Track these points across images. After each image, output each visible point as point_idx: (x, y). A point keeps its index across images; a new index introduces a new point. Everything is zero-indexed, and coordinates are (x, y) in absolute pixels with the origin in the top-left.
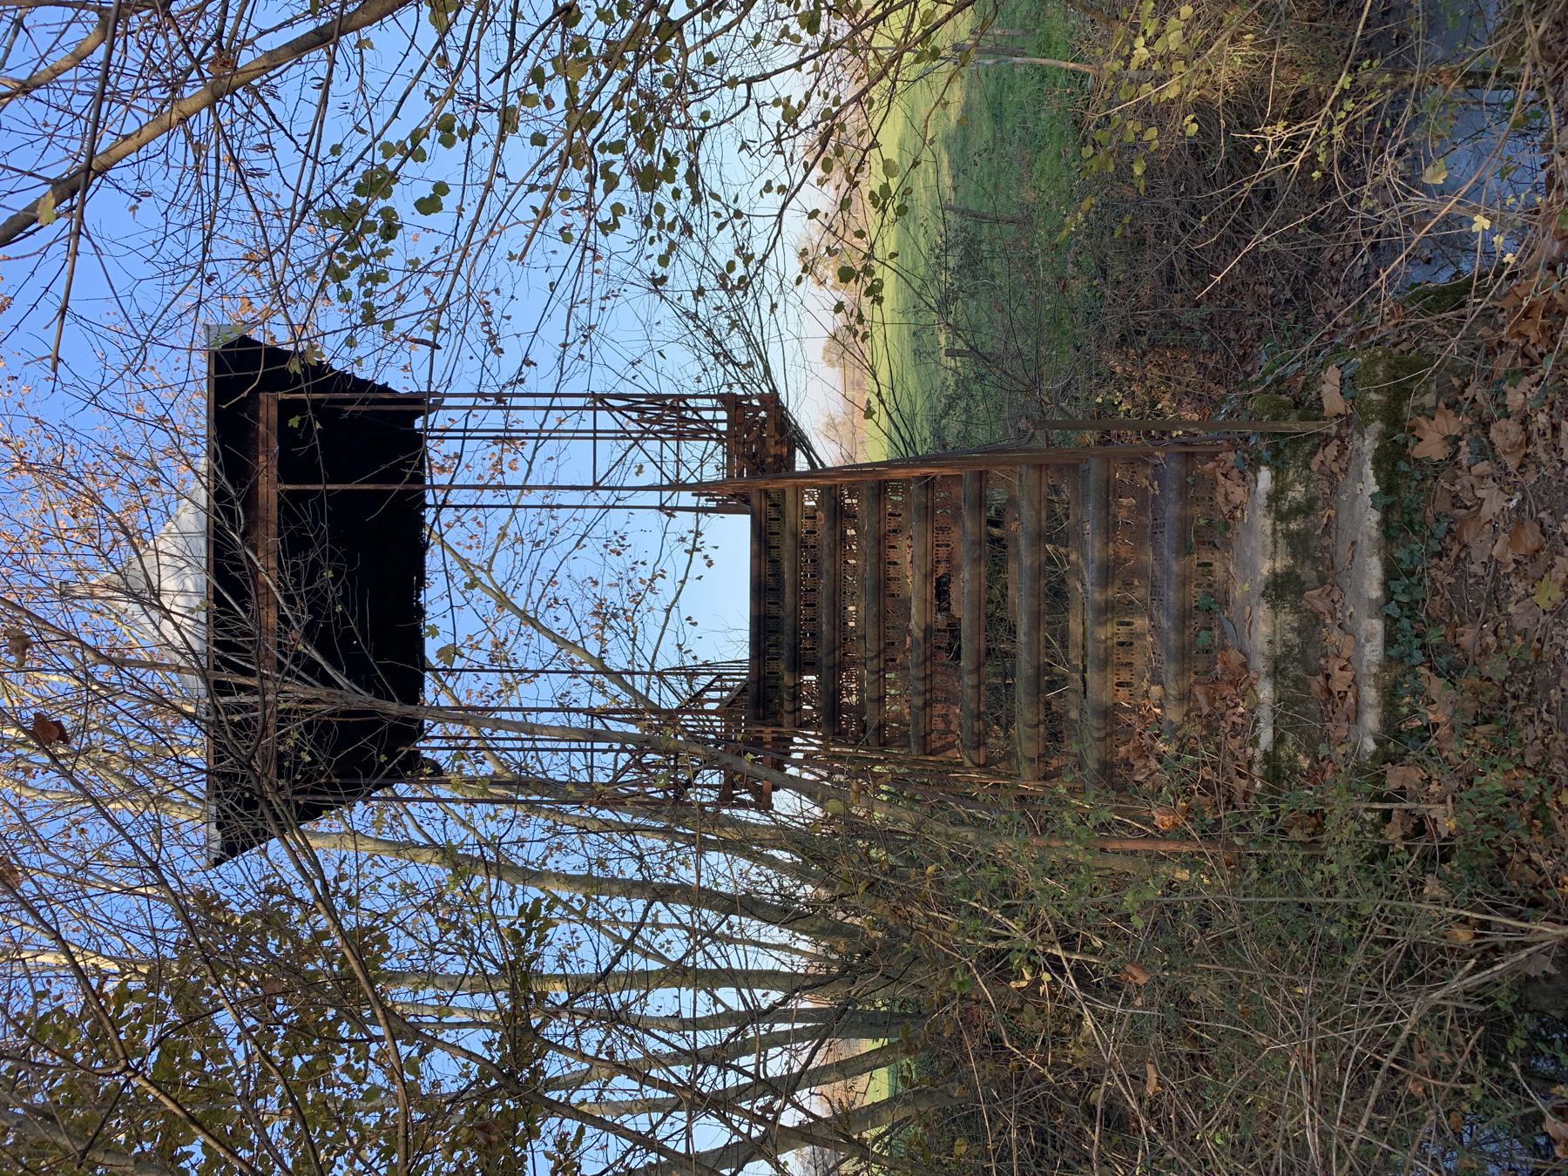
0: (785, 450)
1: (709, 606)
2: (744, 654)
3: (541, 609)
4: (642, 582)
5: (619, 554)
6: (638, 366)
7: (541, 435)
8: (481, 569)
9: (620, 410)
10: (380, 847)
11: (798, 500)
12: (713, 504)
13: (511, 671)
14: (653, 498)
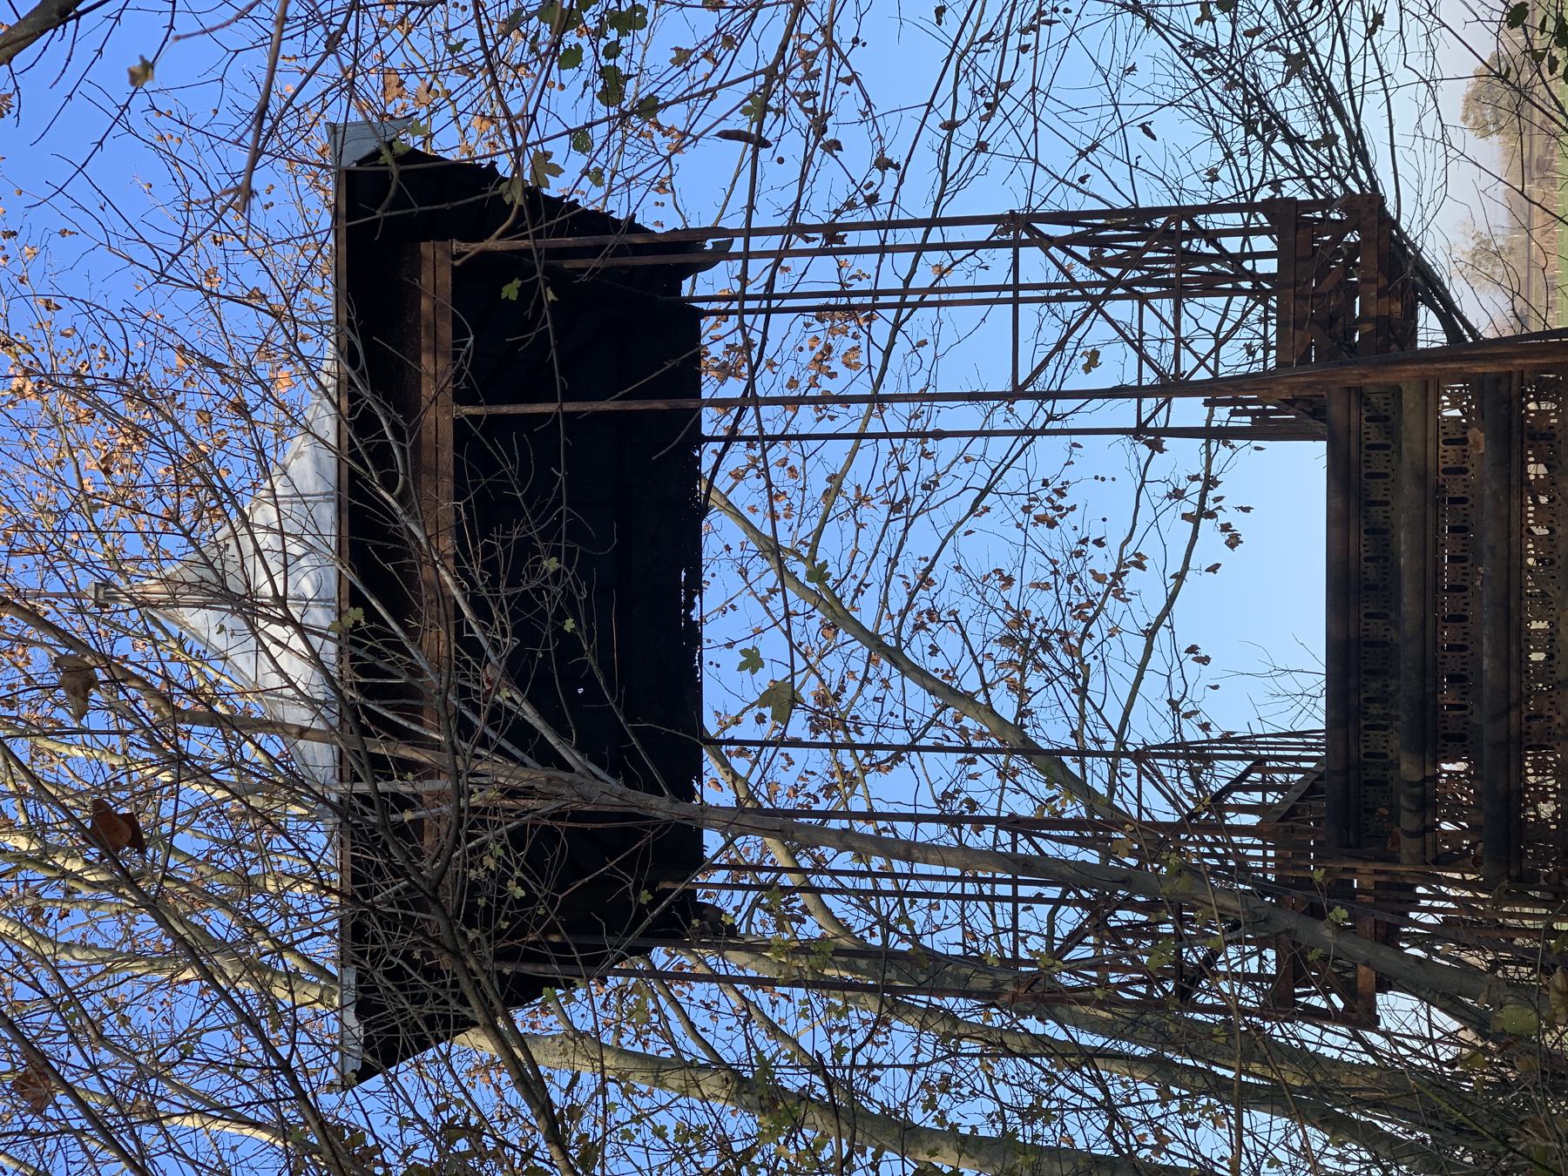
0: (1397, 307)
1: (1245, 613)
2: (1315, 719)
3: (905, 635)
4: (1099, 578)
5: (1052, 524)
6: (1097, 156)
7: (907, 300)
8: (797, 553)
9: (1062, 243)
10: (629, 1064)
11: (1430, 405)
12: (1246, 421)
13: (853, 747)
14: (1123, 413)
